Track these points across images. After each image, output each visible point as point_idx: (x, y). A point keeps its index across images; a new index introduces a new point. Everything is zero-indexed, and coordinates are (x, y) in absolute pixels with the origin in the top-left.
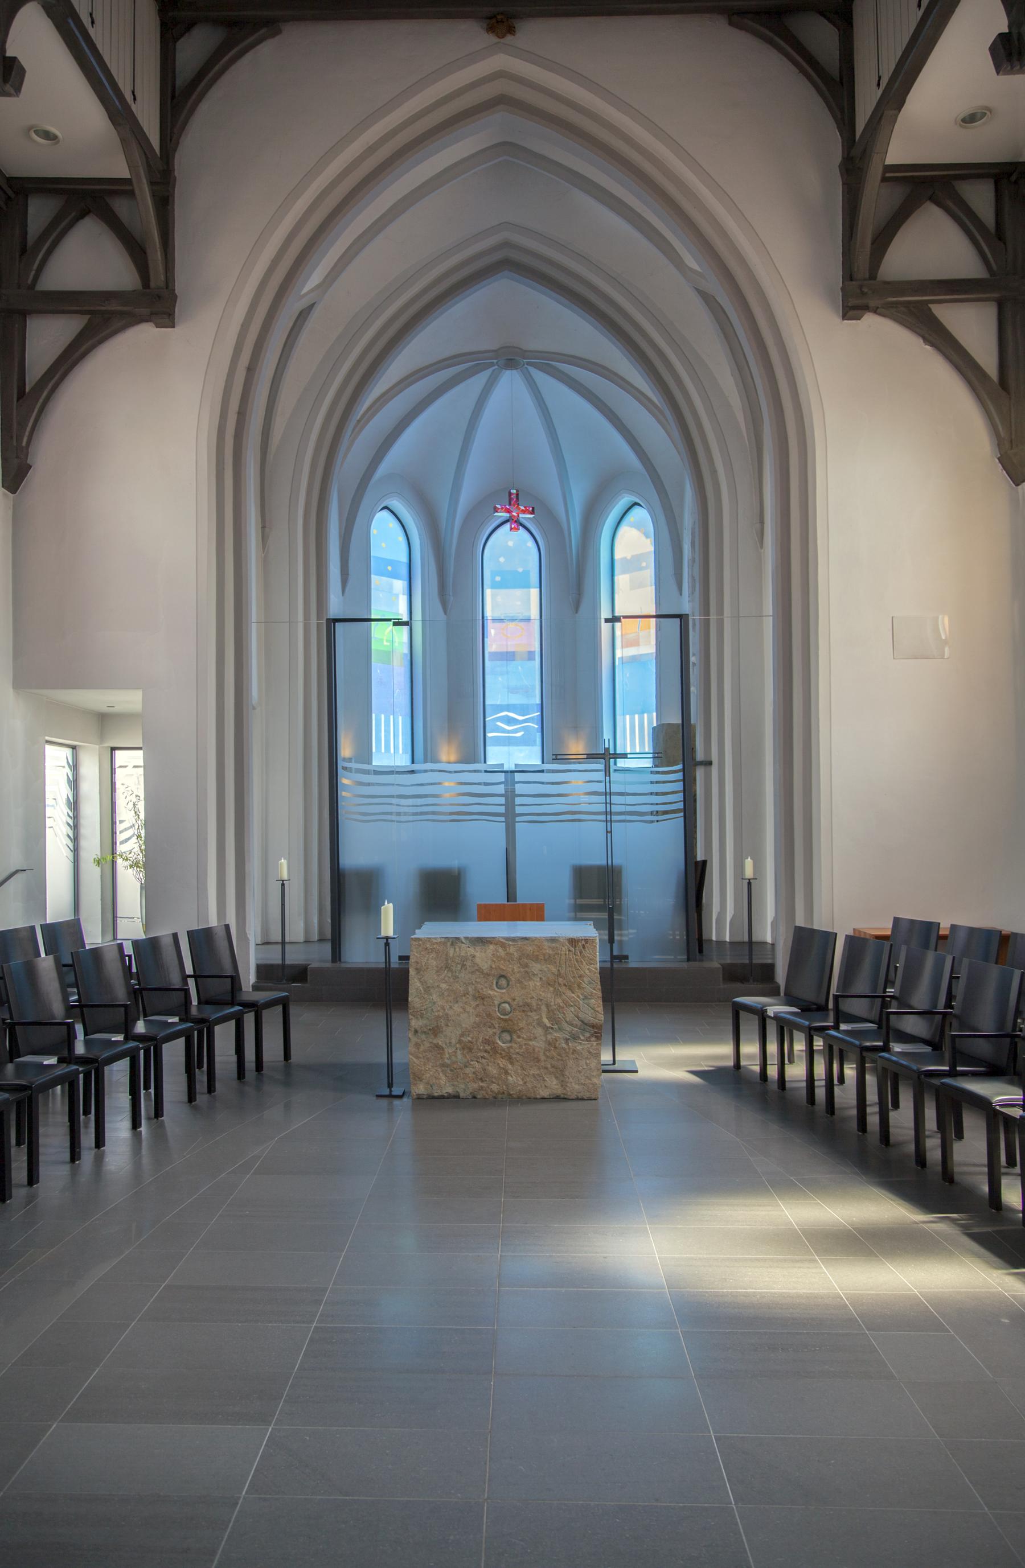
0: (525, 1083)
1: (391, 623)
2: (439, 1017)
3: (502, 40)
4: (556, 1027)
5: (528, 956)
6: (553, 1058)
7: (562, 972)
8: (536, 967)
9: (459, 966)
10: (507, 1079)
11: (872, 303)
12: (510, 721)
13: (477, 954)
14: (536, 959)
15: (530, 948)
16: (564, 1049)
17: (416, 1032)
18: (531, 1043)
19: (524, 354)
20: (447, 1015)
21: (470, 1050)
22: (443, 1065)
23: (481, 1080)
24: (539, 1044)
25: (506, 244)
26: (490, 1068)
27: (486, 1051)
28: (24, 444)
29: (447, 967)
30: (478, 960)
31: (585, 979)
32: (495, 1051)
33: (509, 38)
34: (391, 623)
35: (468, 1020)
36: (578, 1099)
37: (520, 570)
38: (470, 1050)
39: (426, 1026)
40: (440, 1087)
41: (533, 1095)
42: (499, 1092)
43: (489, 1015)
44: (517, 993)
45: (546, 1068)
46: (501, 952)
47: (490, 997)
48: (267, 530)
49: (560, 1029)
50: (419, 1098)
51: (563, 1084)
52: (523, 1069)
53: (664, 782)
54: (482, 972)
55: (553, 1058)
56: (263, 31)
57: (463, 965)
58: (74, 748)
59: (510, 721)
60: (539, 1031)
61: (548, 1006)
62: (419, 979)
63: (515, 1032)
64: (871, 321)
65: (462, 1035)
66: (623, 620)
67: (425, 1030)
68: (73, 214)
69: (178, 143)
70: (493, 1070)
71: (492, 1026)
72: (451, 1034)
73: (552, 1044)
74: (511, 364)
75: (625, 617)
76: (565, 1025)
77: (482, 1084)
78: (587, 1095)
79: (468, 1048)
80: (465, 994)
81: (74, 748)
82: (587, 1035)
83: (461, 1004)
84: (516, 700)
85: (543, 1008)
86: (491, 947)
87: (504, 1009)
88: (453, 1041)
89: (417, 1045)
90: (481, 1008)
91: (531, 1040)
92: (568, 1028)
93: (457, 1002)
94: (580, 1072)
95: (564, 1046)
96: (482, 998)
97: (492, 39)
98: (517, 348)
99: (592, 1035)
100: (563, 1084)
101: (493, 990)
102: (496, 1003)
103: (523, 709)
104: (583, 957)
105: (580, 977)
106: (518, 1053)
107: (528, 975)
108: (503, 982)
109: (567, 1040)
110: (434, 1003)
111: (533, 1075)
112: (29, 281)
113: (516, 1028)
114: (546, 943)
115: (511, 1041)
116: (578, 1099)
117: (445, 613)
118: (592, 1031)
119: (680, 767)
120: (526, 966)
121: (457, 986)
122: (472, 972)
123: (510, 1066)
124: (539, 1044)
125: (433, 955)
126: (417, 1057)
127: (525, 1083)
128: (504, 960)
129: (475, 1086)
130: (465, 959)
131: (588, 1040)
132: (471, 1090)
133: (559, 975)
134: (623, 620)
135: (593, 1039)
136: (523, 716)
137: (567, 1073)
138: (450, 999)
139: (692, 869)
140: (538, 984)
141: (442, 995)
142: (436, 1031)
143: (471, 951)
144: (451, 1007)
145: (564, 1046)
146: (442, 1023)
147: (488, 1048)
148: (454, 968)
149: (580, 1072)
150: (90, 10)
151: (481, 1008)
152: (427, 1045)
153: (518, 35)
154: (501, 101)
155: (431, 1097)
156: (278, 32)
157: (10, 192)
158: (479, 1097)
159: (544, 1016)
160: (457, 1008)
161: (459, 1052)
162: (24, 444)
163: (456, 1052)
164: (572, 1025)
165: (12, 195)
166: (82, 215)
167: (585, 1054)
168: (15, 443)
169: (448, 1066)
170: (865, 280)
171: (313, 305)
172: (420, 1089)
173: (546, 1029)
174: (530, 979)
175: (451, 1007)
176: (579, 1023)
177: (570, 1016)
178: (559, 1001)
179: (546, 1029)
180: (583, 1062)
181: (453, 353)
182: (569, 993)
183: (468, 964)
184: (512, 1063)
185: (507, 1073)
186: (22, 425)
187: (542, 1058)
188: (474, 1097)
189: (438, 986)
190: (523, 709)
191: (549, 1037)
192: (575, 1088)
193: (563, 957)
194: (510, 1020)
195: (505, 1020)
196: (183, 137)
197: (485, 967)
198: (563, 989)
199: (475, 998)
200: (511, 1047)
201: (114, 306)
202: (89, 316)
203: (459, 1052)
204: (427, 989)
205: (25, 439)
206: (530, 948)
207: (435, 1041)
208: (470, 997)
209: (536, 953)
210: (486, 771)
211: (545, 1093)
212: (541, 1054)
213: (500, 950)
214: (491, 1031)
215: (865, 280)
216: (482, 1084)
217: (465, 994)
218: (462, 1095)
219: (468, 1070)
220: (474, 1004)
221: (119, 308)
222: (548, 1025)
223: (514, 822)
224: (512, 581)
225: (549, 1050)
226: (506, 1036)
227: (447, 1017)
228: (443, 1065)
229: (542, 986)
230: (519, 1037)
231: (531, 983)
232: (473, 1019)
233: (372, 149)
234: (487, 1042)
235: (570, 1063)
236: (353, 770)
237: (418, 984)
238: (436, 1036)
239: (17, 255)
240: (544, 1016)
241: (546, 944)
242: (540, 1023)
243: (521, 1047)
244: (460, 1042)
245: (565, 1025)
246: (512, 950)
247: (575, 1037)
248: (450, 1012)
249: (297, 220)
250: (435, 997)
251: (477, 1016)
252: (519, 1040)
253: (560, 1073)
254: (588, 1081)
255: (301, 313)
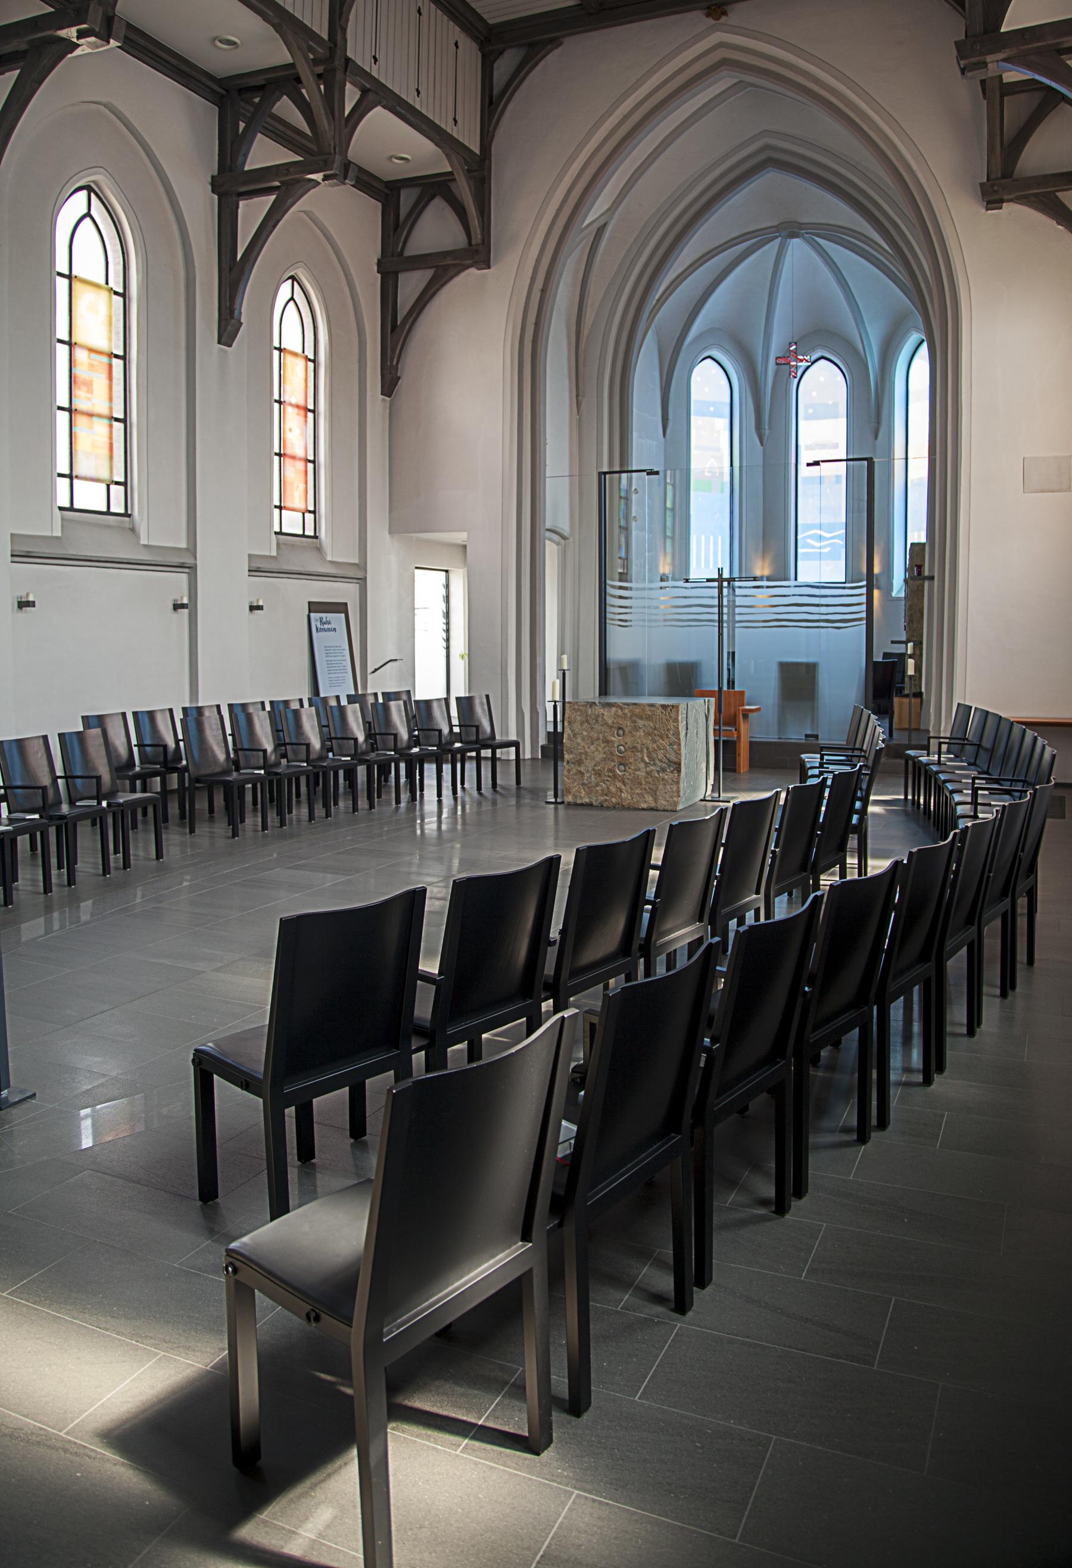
0: (632, 798)
1: (645, 473)
2: (581, 753)
3: (719, 22)
4: (652, 763)
5: (636, 716)
6: (649, 783)
7: (657, 726)
8: (641, 723)
9: (594, 721)
10: (621, 795)
11: (1006, 197)
12: (820, 538)
13: (605, 714)
14: (641, 718)
15: (638, 710)
16: (657, 778)
17: (568, 762)
18: (637, 773)
19: (801, 226)
20: (586, 752)
21: (600, 775)
22: (583, 784)
23: (606, 795)
24: (641, 774)
25: (767, 147)
26: (611, 787)
27: (609, 776)
28: (395, 363)
29: (587, 721)
30: (605, 717)
31: (671, 732)
32: (615, 777)
33: (724, 19)
34: (645, 473)
35: (599, 756)
36: (664, 810)
37: (830, 402)
38: (600, 775)
39: (574, 758)
40: (581, 798)
41: (637, 806)
42: (616, 803)
43: (611, 753)
44: (629, 740)
45: (646, 789)
46: (620, 712)
47: (612, 742)
48: (580, 398)
49: (655, 764)
50: (569, 804)
51: (656, 800)
52: (631, 789)
53: (852, 596)
54: (608, 725)
55: (649, 783)
56: (549, 47)
57: (597, 720)
58: (447, 571)
59: (820, 538)
60: (642, 765)
61: (648, 749)
62: (570, 729)
63: (627, 764)
64: (1011, 209)
65: (595, 765)
66: (821, 464)
67: (573, 761)
68: (426, 199)
69: (493, 136)
70: (613, 789)
71: (613, 761)
72: (589, 764)
73: (649, 773)
74: (793, 235)
75: (823, 461)
76: (657, 762)
77: (606, 798)
78: (670, 808)
79: (598, 774)
80: (598, 739)
81: (447, 571)
82: (672, 769)
83: (595, 745)
84: (826, 519)
85: (645, 750)
86: (614, 709)
87: (621, 749)
88: (590, 769)
89: (569, 771)
90: (607, 749)
91: (636, 771)
92: (659, 764)
93: (593, 744)
94: (666, 793)
95: (657, 775)
96: (607, 742)
97: (711, 21)
98: (795, 222)
99: (675, 769)
100: (656, 800)
101: (614, 737)
102: (616, 745)
103: (831, 528)
104: (671, 717)
105: (668, 730)
106: (628, 779)
107: (636, 728)
108: (621, 732)
109: (658, 772)
110: (579, 744)
111: (638, 794)
112: (399, 250)
113: (627, 762)
114: (647, 707)
115: (625, 771)
116: (664, 810)
117: (762, 445)
118: (675, 766)
119: (864, 583)
120: (635, 722)
121: (592, 734)
122: (602, 725)
123: (623, 787)
124: (641, 774)
125: (579, 713)
126: (569, 779)
127: (632, 798)
128: (621, 717)
129: (602, 798)
130: (598, 716)
131: (672, 772)
132: (600, 801)
133: (655, 729)
134: (821, 464)
135: (675, 772)
136: (830, 533)
137: (658, 793)
138: (588, 742)
139: (871, 666)
140: (642, 734)
141: (583, 739)
142: (580, 762)
143: (602, 711)
144: (589, 747)
145: (657, 775)
146: (583, 757)
147: (611, 774)
148: (591, 722)
149: (666, 793)
150: (416, 87)
151: (607, 749)
152: (574, 771)
153: (730, 15)
154: (724, 63)
155: (576, 804)
156: (561, 44)
157: (387, 191)
158: (605, 806)
159: (645, 755)
160: (592, 748)
161: (593, 776)
162: (395, 363)
163: (590, 776)
164: (662, 762)
165: (389, 192)
166: (432, 198)
167: (670, 781)
168: (389, 364)
169: (586, 785)
170: (998, 179)
171: (605, 224)
172: (569, 798)
173: (646, 764)
174: (638, 731)
175: (589, 747)
176: (666, 761)
177: (660, 756)
178: (655, 746)
179: (646, 764)
180: (668, 787)
181: (705, 250)
182: (661, 741)
183: (600, 719)
184: (624, 785)
185: (621, 791)
186: (393, 350)
187: (644, 783)
188: (602, 806)
189: (581, 733)
190: (831, 528)
191: (648, 769)
192: (662, 803)
193: (658, 717)
194: (624, 757)
195: (621, 757)
196: (497, 131)
197: (610, 722)
198: (657, 738)
199: (604, 742)
200: (624, 775)
201: (449, 261)
202: (434, 269)
203: (593, 776)
204: (575, 735)
205: (395, 360)
206: (638, 710)
207: (579, 769)
208: (601, 742)
209: (641, 714)
210: (795, 586)
211: (645, 806)
212: (643, 780)
213: (619, 711)
214: (612, 764)
215: (998, 179)
216: (606, 798)
217: (598, 739)
218: (594, 803)
219: (598, 788)
220: (603, 745)
221: (452, 262)
222: (647, 761)
223: (734, 628)
224: (823, 413)
225: (648, 778)
226: (622, 768)
227: (586, 753)
228: (583, 784)
229: (645, 735)
230: (629, 768)
231: (638, 734)
232: (602, 755)
233: (626, 117)
234: (610, 770)
235: (661, 787)
236: (765, 579)
237: (570, 732)
238: (579, 765)
239: (392, 233)
240: (645, 755)
241: (647, 708)
242: (643, 760)
243: (630, 775)
244: (594, 770)
245: (657, 762)
246: (626, 711)
247: (664, 770)
248: (588, 750)
249: (574, 178)
250: (579, 740)
251: (604, 753)
252: (629, 770)
253: (654, 793)
254: (671, 799)
255: (599, 229)
